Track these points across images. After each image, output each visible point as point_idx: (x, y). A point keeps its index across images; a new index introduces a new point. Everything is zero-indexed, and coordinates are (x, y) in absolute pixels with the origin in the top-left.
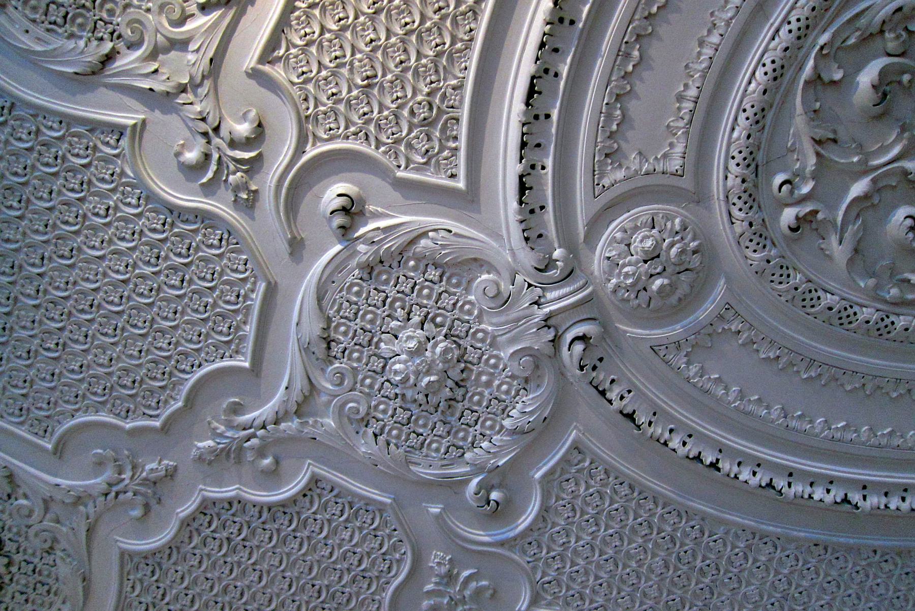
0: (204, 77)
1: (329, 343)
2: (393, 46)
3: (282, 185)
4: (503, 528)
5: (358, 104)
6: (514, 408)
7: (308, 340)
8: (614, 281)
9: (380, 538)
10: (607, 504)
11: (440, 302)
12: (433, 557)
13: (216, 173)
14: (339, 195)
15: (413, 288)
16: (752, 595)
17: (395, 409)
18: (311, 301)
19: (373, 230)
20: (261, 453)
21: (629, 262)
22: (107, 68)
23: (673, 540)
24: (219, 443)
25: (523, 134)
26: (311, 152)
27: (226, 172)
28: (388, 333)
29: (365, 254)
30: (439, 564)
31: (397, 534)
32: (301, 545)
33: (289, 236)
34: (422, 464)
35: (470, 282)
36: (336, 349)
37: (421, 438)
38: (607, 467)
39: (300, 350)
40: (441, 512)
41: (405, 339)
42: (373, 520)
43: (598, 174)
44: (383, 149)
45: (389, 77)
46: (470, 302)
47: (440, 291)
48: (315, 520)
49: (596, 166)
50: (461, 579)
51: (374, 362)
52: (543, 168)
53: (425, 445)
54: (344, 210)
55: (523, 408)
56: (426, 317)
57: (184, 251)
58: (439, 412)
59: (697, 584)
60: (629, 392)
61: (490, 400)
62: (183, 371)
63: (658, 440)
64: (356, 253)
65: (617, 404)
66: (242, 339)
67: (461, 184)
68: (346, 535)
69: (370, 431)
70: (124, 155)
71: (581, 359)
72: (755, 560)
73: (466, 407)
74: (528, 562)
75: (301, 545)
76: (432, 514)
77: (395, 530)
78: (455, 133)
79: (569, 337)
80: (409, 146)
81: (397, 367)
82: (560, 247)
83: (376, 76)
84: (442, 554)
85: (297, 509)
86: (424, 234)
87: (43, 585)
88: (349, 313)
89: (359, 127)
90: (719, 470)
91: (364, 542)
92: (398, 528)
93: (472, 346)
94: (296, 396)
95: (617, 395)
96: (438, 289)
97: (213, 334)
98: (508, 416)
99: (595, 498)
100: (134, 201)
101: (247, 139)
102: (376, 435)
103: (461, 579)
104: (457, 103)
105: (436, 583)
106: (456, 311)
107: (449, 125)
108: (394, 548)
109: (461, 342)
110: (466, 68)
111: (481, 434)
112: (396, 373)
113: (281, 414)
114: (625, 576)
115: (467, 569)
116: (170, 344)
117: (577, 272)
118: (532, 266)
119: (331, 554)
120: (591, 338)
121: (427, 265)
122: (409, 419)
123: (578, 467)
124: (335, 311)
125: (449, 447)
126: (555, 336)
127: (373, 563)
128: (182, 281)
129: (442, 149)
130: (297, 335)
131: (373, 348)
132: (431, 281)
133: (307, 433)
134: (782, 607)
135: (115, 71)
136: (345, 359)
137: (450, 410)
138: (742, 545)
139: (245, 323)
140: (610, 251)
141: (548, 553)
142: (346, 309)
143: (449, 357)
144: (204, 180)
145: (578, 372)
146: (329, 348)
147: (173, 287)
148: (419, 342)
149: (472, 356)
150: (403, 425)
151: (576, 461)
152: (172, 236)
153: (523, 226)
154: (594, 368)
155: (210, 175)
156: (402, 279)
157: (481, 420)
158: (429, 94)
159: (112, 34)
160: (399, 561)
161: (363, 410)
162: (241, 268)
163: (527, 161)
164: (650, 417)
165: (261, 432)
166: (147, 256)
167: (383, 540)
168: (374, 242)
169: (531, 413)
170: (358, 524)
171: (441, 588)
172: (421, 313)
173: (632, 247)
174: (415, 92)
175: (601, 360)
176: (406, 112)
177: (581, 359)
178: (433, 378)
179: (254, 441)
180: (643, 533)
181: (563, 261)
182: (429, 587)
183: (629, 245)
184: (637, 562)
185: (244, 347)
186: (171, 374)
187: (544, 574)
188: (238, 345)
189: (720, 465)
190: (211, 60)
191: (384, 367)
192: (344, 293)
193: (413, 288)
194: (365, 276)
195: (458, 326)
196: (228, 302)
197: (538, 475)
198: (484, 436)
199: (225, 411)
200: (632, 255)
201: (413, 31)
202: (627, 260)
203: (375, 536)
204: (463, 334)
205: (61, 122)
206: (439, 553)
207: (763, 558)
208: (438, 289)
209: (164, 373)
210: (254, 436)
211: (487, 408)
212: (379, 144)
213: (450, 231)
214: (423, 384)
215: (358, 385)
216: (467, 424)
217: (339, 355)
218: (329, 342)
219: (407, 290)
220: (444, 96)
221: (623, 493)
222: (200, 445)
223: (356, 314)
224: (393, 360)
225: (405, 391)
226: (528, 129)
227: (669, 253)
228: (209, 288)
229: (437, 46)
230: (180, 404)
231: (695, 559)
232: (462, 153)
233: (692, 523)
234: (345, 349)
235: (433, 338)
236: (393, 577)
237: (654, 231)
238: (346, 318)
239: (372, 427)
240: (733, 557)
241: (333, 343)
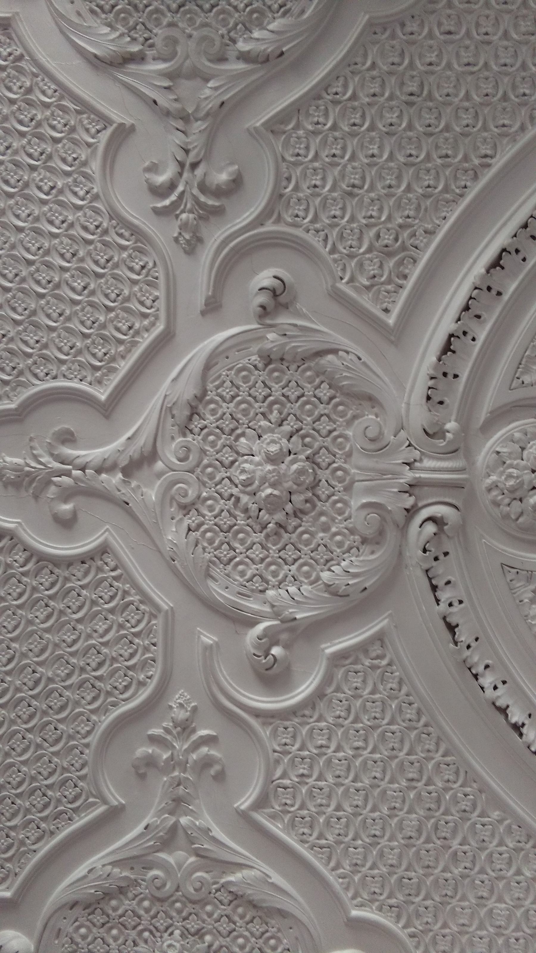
0: (208, 114)
1: (192, 415)
2: (390, 169)
3: (227, 245)
4: (268, 697)
5: (333, 205)
6: (338, 564)
7: (175, 400)
8: (494, 478)
9: (135, 647)
10: (385, 721)
11: (317, 423)
12: (177, 696)
13: (173, 203)
14: (275, 277)
15: (299, 398)
16: (499, 915)
17: (223, 511)
18: (198, 365)
19: (290, 324)
21: (517, 464)
22: (127, 66)
23: (438, 801)
24: (28, 465)
25: (471, 298)
26: (269, 227)
27: (182, 207)
28: (254, 430)
29: (272, 342)
30: (181, 705)
31: (155, 651)
32: (49, 617)
33: (210, 293)
34: (220, 581)
35: (355, 417)
36: (197, 424)
37: (232, 553)
38: (405, 678)
39: (162, 409)
40: (212, 645)
41: (268, 441)
42: (139, 622)
43: (523, 368)
44: (336, 256)
45: (372, 195)
46: (346, 438)
47: (322, 412)
48: (79, 595)
49: (524, 360)
50: (194, 737)
51: (226, 453)
52: (474, 339)
53: (232, 564)
54: (274, 293)
55: (348, 567)
56: (298, 431)
57: (102, 261)
58: (263, 535)
59: (443, 871)
60: (461, 602)
61: (319, 545)
62: (36, 376)
63: (470, 669)
64: (263, 338)
65: (443, 606)
66: (113, 370)
67: (391, 320)
68: (101, 627)
69: (187, 522)
70: (96, 148)
71: (428, 542)
72: (519, 872)
73: (292, 541)
74: (275, 751)
75: (49, 617)
76: (202, 642)
77: (154, 645)
78: (407, 271)
79: (425, 513)
80: (361, 265)
81: (247, 466)
82: (456, 421)
83: (361, 188)
84: (188, 697)
85: (66, 574)
86: (334, 351)
88: (228, 393)
89: (324, 226)
90: (521, 735)
91: (117, 644)
92: (160, 644)
93: (327, 481)
94: (134, 451)
95: (447, 599)
96: (322, 409)
97: (86, 352)
98: (329, 570)
99: (376, 707)
100: (81, 193)
102: (189, 530)
103: (194, 737)
104: (422, 245)
105: (167, 730)
106: (329, 439)
107: (405, 262)
108: (144, 665)
109: (319, 472)
110: (445, 218)
111: (293, 577)
112: (243, 471)
113: (109, 463)
114: (369, 821)
115: (206, 728)
116: (37, 342)
117: (461, 453)
118: (422, 425)
119: (75, 642)
120: (447, 524)
121: (322, 382)
122: (231, 527)
123: (374, 661)
124: (215, 386)
125: (254, 576)
126: (413, 507)
127: (112, 674)
128: (85, 288)
129: (389, 281)
130: (167, 390)
131: (232, 438)
132: (319, 399)
133: (123, 494)
134: (526, 947)
135: (130, 71)
136: (200, 438)
137: (275, 537)
138: (511, 845)
139: (123, 357)
140: (503, 447)
141: (299, 750)
142: (227, 388)
143: (302, 478)
144: (159, 205)
145: (420, 552)
146: (190, 418)
147: (73, 289)
148: (281, 449)
149: (323, 491)
150: (222, 531)
151: (374, 654)
152: (99, 241)
153: (431, 383)
154: (436, 559)
155: (167, 202)
156: (293, 384)
157: (301, 561)
158: (401, 226)
159: (146, 40)
160: (142, 684)
161: (192, 494)
162: (148, 303)
163: (463, 324)
164: (471, 640)
165: (77, 473)
166: (64, 248)
167: (136, 651)
168: (285, 335)
169: (355, 575)
170: (121, 620)
171: (169, 737)
172: (295, 424)
173: (525, 453)
174: (390, 218)
175: (446, 554)
176: (372, 232)
177: (428, 542)
178: (276, 492)
179: (65, 479)
180: (411, 776)
181: (453, 434)
182: (157, 731)
183: (523, 449)
184: (390, 809)
185: (109, 380)
186: (21, 373)
187: (284, 775)
188: (104, 375)
189: (524, 730)
190: (223, 103)
191: (233, 463)
192: (233, 372)
193: (299, 398)
194: (260, 365)
195: (324, 455)
196: (118, 329)
197: (329, 651)
198: (295, 580)
199: (54, 434)
200: (522, 460)
201: (413, 165)
202: (515, 462)
203: (131, 642)
204: (324, 465)
205: (55, 91)
206: (186, 694)
207: (528, 874)
208: (322, 409)
209: (14, 368)
210: (68, 474)
211: (312, 552)
212: (334, 250)
213: (360, 359)
214: (263, 495)
215: (199, 470)
216: (284, 560)
217: (197, 430)
218: (194, 412)
219: (293, 397)
220: (413, 235)
221: (408, 716)
222: (8, 459)
223: (233, 397)
224: (246, 457)
225: (241, 495)
226: (478, 294)
228: (106, 306)
229: (429, 186)
230: (13, 406)
231: (454, 837)
232: (404, 294)
233: (468, 790)
234: (206, 427)
235: (295, 454)
236: (124, 700)
238: (222, 397)
239: (190, 519)
240: (496, 856)
241: (196, 416)
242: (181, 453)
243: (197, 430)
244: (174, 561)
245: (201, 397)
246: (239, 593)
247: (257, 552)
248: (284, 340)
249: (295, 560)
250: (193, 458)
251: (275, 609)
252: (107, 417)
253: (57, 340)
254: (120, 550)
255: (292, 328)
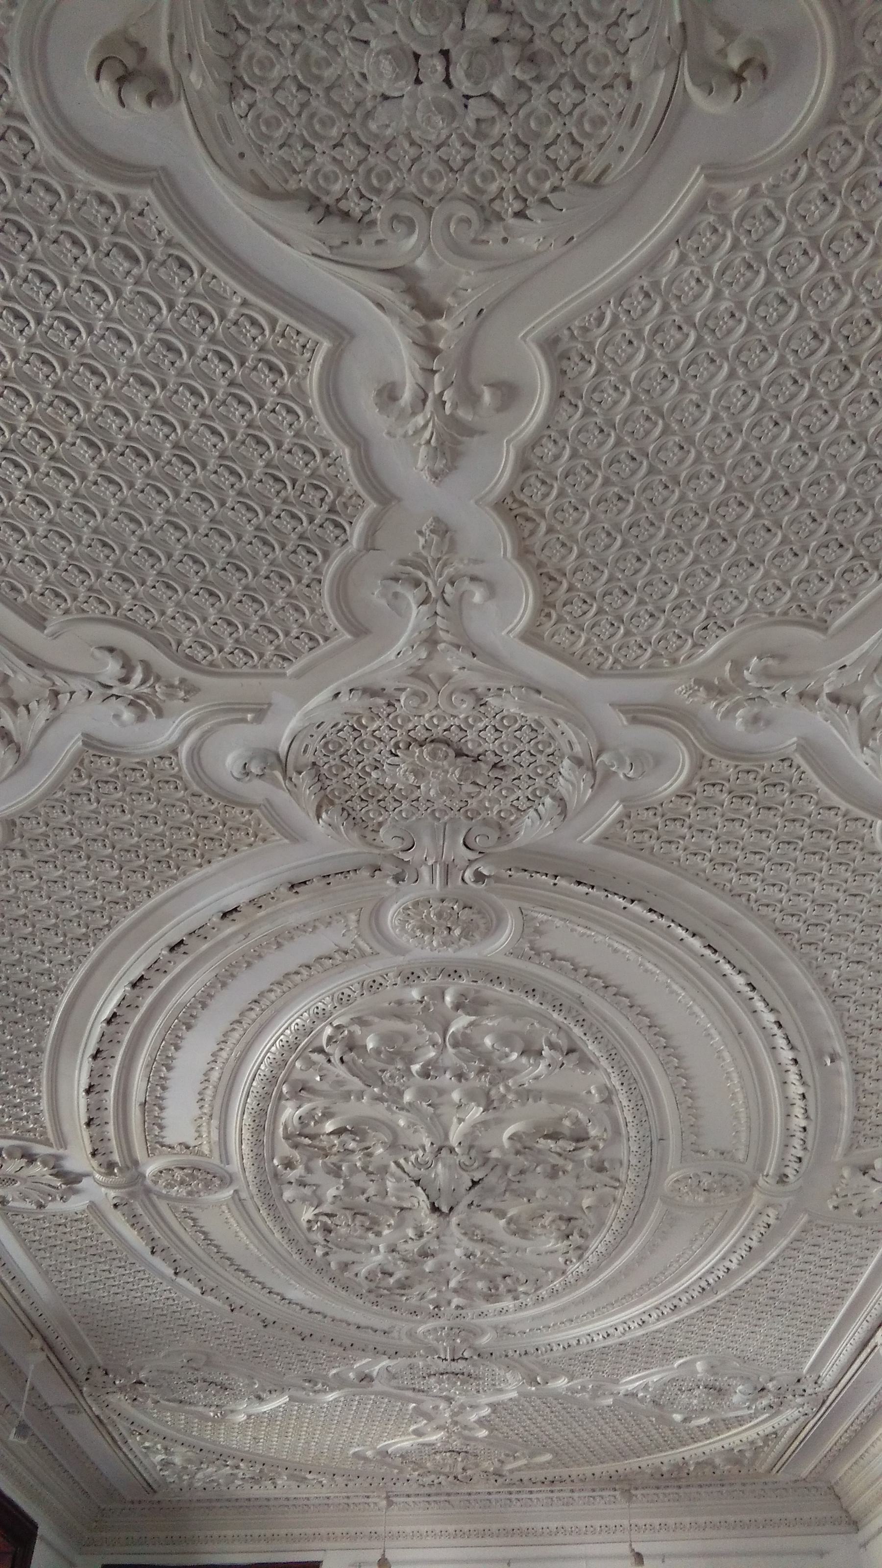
14: (98, 78)
20: (470, 397)
24: (428, 442)
36: (355, 207)
87: (556, 105)
101: (123, 667)
146: (346, 215)
161: (465, 211)
190: (29, 665)
217: (364, 205)
227: (420, 35)
230: (347, 451)
237: (373, 44)
242: (401, 229)
243: (364, 205)
244: (572, 238)
245: (313, 202)
246: (633, 124)
247: (567, 96)
248: (198, 57)
249: (580, 24)
250: (408, 210)
251: (662, 63)
252: (352, 336)
253: (866, 488)
254: (540, 329)
255: (176, 48)
